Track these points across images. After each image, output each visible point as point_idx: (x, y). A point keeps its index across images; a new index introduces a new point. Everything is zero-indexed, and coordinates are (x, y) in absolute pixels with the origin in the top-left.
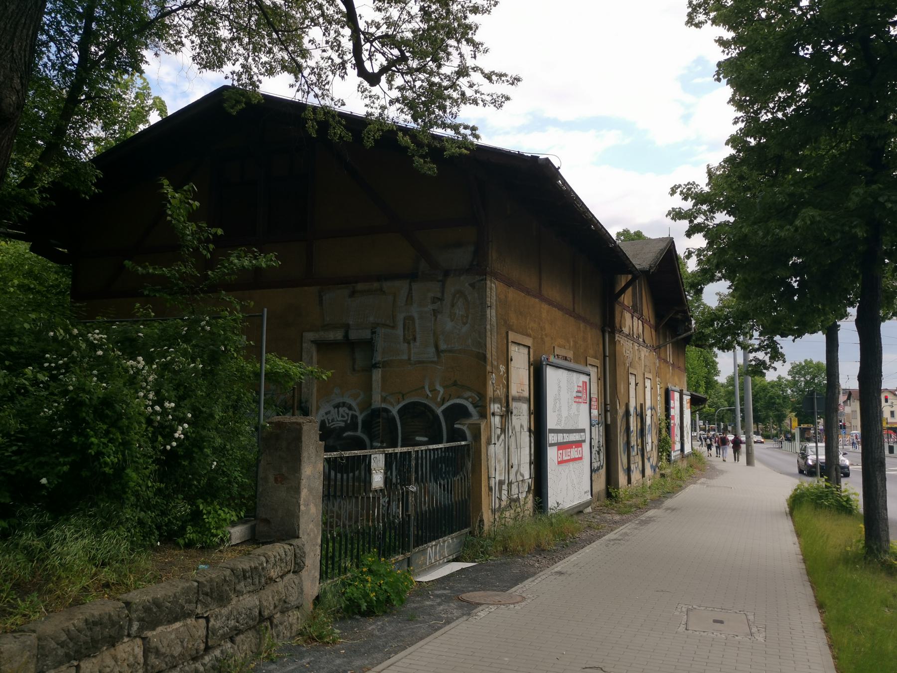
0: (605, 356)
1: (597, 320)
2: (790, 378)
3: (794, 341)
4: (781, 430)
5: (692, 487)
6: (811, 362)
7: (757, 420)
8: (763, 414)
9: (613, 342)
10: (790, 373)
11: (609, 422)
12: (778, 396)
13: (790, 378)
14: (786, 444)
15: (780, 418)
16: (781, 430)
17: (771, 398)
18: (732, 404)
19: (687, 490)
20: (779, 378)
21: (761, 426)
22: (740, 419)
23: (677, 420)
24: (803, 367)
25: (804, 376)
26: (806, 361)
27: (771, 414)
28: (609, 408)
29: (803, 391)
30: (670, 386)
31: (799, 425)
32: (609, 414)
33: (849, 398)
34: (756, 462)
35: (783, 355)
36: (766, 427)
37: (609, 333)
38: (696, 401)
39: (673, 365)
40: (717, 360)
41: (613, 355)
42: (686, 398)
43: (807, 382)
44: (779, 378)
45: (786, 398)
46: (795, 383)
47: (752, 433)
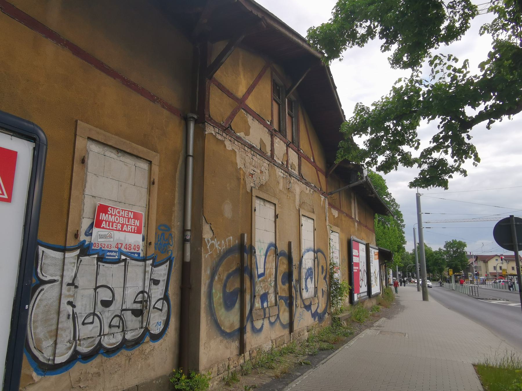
0: (187, 156)
1: (169, 91)
2: (445, 249)
3: (488, 127)
4: (441, 277)
5: (368, 332)
6: (456, 241)
7: (429, 271)
8: (431, 268)
9: (200, 135)
10: (445, 247)
11: (188, 258)
12: (440, 259)
13: (445, 249)
14: (446, 284)
15: (441, 270)
16: (441, 277)
17: (436, 260)
18: (415, 262)
19: (362, 335)
20: (440, 249)
21: (431, 274)
22: (419, 270)
23: (363, 267)
24: (452, 244)
25: (452, 248)
26: (453, 240)
27: (436, 268)
28: (188, 235)
29: (452, 256)
30: (354, 237)
31: (454, 273)
32: (188, 246)
33: (476, 260)
34: (429, 297)
35: (472, 148)
36: (433, 275)
37: (196, 122)
38: (385, 257)
39: (359, 223)
40: (404, 235)
41: (200, 156)
42: (374, 252)
43: (454, 252)
44: (440, 249)
45: (443, 259)
46: (447, 252)
47: (426, 278)
